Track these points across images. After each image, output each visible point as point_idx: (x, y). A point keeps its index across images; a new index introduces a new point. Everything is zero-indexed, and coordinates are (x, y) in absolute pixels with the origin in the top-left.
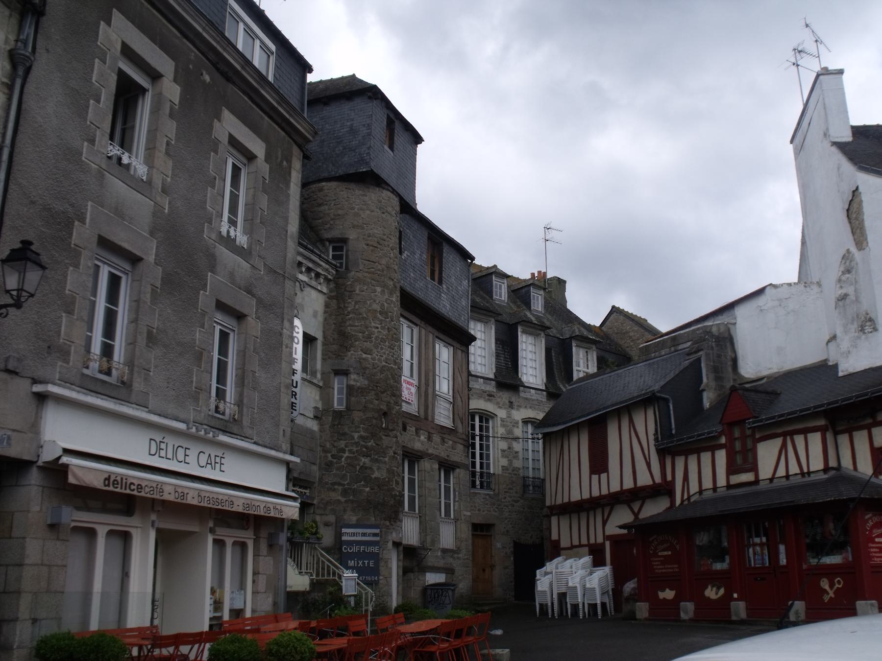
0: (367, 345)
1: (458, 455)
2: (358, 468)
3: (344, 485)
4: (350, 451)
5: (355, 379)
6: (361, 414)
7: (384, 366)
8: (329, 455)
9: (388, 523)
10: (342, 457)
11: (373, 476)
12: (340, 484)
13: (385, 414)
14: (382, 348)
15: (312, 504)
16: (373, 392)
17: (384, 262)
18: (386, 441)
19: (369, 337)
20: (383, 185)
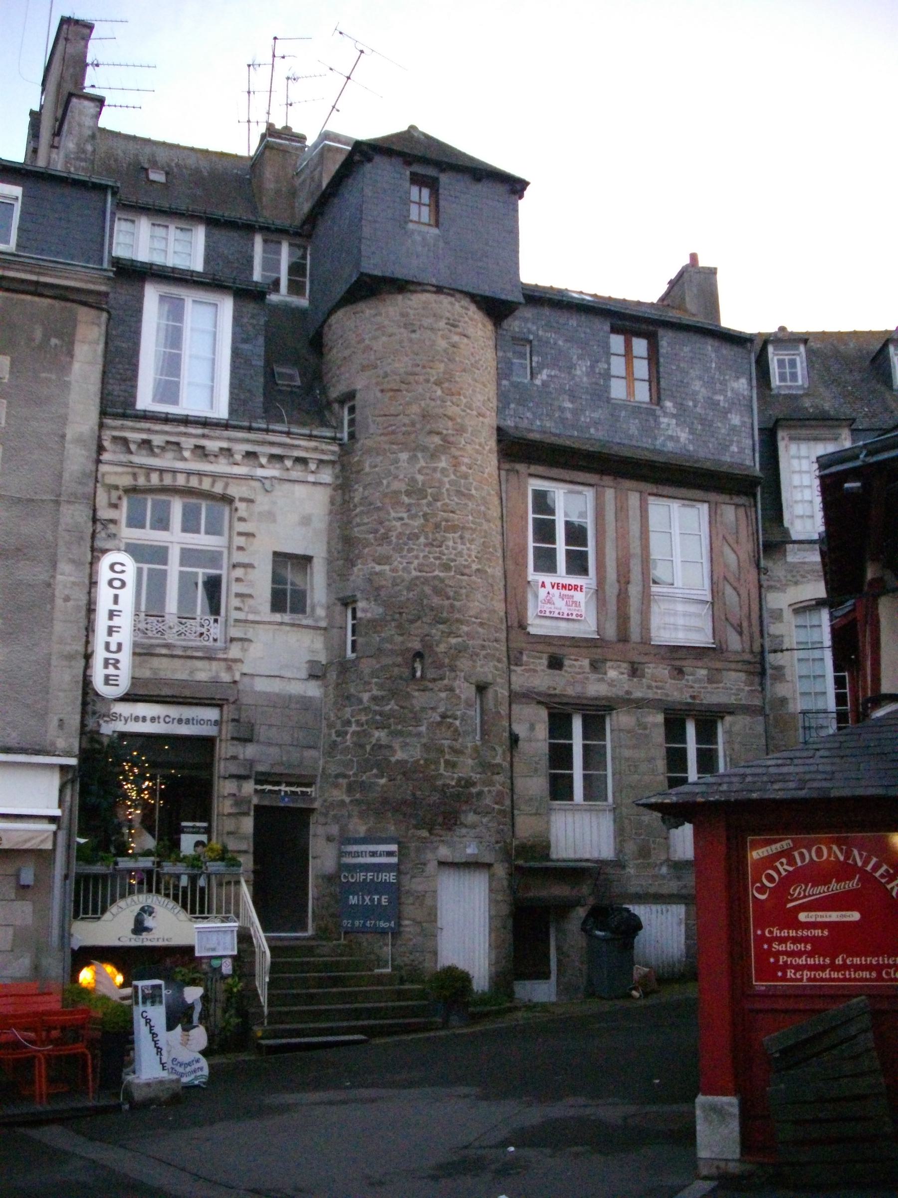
0: (384, 550)
1: (733, 687)
2: (368, 748)
3: (349, 777)
4: (357, 722)
5: (366, 609)
6: (373, 661)
7: (417, 578)
8: (333, 731)
9: (424, 833)
10: (346, 733)
11: (393, 759)
12: (345, 776)
13: (419, 655)
14: (410, 550)
15: (314, 809)
16: (393, 624)
17: (415, 409)
18: (419, 699)
19: (386, 538)
20: (412, 288)
